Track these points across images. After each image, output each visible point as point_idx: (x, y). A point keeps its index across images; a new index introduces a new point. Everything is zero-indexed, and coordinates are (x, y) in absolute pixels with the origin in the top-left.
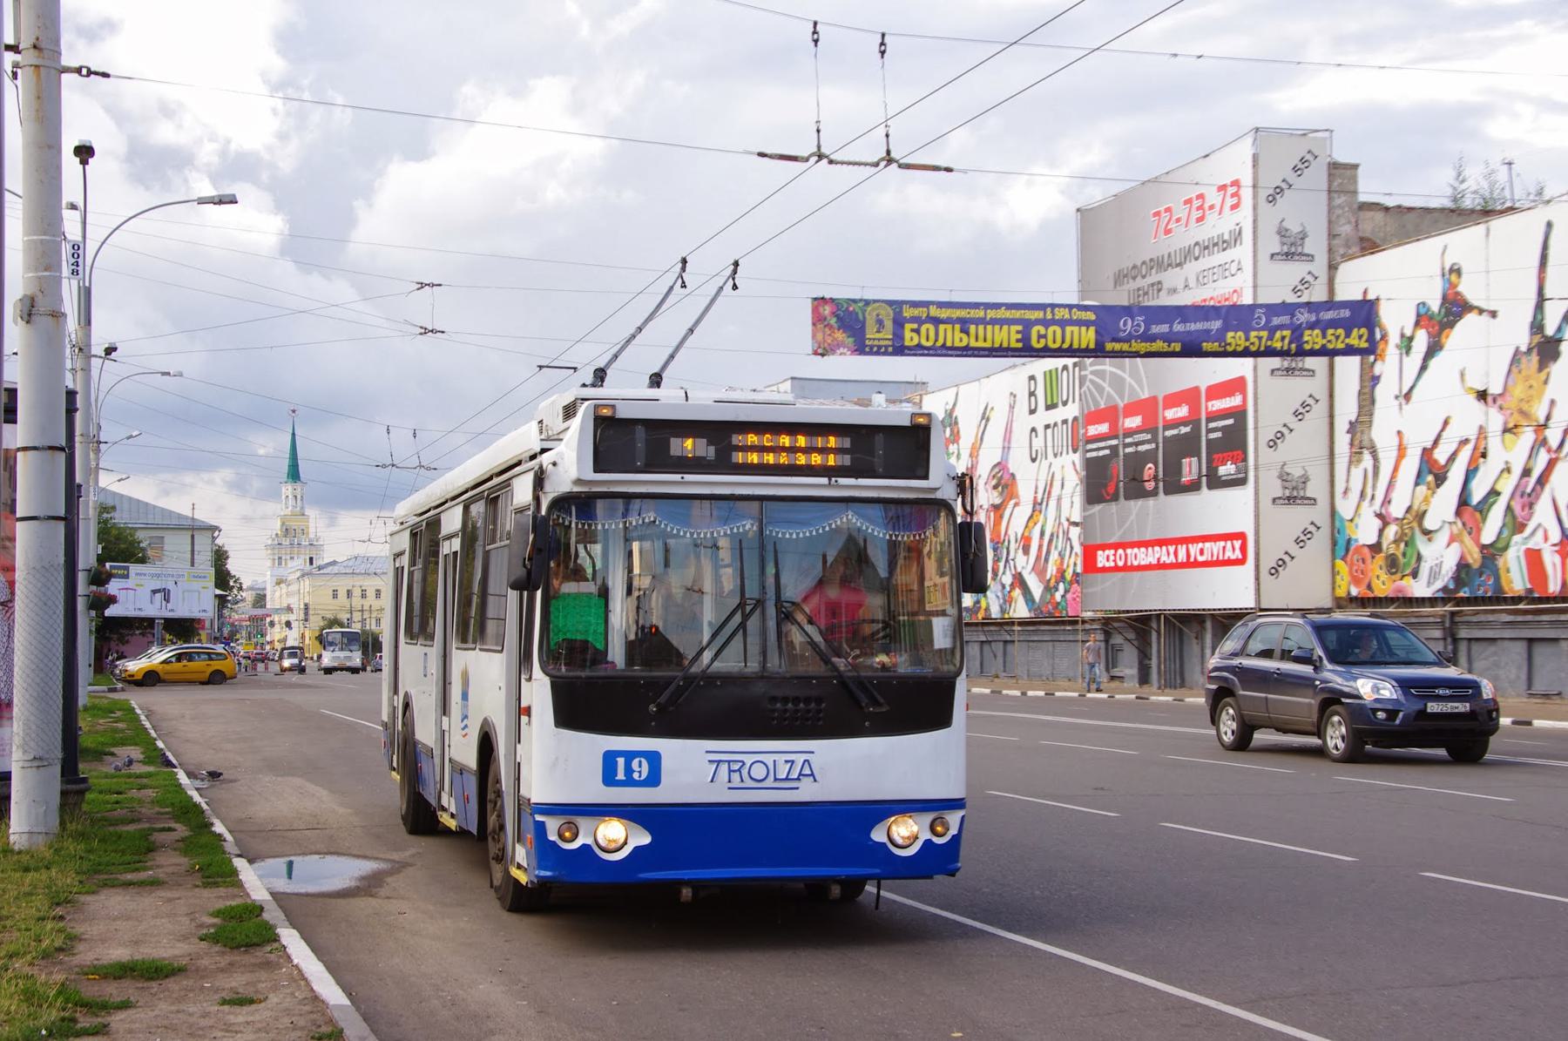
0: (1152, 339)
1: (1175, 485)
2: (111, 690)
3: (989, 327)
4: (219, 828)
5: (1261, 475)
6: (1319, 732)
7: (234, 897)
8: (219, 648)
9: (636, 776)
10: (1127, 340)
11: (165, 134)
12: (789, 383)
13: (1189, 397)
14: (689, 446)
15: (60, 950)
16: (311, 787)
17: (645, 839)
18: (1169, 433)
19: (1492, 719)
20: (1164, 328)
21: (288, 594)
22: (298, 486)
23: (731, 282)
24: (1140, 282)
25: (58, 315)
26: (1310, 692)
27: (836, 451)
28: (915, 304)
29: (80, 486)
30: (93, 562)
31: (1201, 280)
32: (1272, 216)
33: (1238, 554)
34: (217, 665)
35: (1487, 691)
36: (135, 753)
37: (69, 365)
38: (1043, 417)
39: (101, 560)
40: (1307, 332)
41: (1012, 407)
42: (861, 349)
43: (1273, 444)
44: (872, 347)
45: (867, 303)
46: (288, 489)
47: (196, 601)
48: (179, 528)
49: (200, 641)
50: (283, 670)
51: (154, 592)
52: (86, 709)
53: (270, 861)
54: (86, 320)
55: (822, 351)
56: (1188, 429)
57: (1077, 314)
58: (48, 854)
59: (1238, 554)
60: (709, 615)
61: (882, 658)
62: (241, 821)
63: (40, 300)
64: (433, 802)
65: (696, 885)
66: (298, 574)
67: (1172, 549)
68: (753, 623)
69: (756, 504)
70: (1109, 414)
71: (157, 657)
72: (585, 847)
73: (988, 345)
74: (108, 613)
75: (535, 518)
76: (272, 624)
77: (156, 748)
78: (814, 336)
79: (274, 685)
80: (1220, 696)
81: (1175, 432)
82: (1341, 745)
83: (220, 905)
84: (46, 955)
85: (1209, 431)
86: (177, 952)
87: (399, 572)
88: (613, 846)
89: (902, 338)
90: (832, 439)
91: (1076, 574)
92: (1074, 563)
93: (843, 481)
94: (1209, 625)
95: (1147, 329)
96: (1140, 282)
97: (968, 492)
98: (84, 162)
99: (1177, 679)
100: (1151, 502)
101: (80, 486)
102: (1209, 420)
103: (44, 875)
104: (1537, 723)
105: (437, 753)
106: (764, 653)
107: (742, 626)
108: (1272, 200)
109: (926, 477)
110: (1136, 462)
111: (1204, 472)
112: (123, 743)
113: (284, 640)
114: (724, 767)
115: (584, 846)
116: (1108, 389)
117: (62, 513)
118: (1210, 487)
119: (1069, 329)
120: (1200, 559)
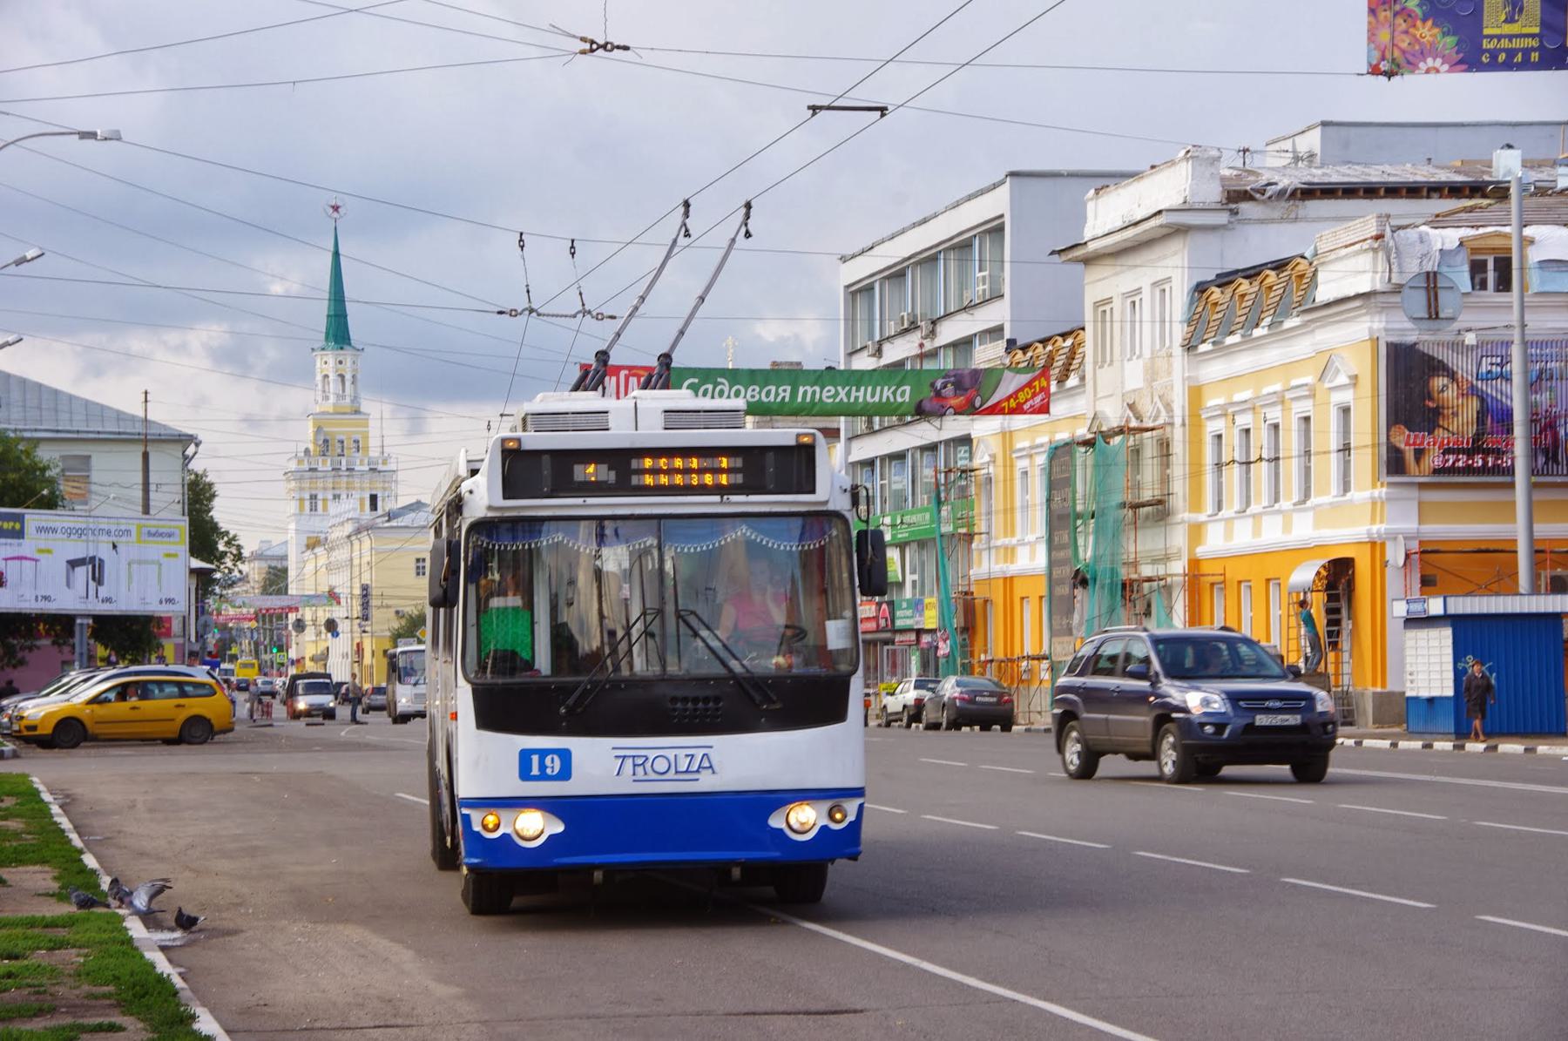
8: (200, 673)
9: (549, 771)
12: (1317, 132)
16: (380, 944)
17: (559, 828)
21: (329, 567)
22: (347, 356)
23: (743, 230)
27: (728, 471)
34: (196, 706)
36: (39, 877)
42: (1472, 58)
44: (1494, 54)
46: (326, 363)
47: (152, 581)
49: (162, 659)
50: (296, 715)
51: (73, 564)
62: (246, 1011)
66: (349, 528)
71: (81, 691)
72: (505, 836)
76: (300, 626)
77: (84, 870)
79: (305, 746)
97: (862, 500)
109: (813, 491)
112: (19, 858)
113: (323, 657)
114: (629, 762)
115: (504, 835)
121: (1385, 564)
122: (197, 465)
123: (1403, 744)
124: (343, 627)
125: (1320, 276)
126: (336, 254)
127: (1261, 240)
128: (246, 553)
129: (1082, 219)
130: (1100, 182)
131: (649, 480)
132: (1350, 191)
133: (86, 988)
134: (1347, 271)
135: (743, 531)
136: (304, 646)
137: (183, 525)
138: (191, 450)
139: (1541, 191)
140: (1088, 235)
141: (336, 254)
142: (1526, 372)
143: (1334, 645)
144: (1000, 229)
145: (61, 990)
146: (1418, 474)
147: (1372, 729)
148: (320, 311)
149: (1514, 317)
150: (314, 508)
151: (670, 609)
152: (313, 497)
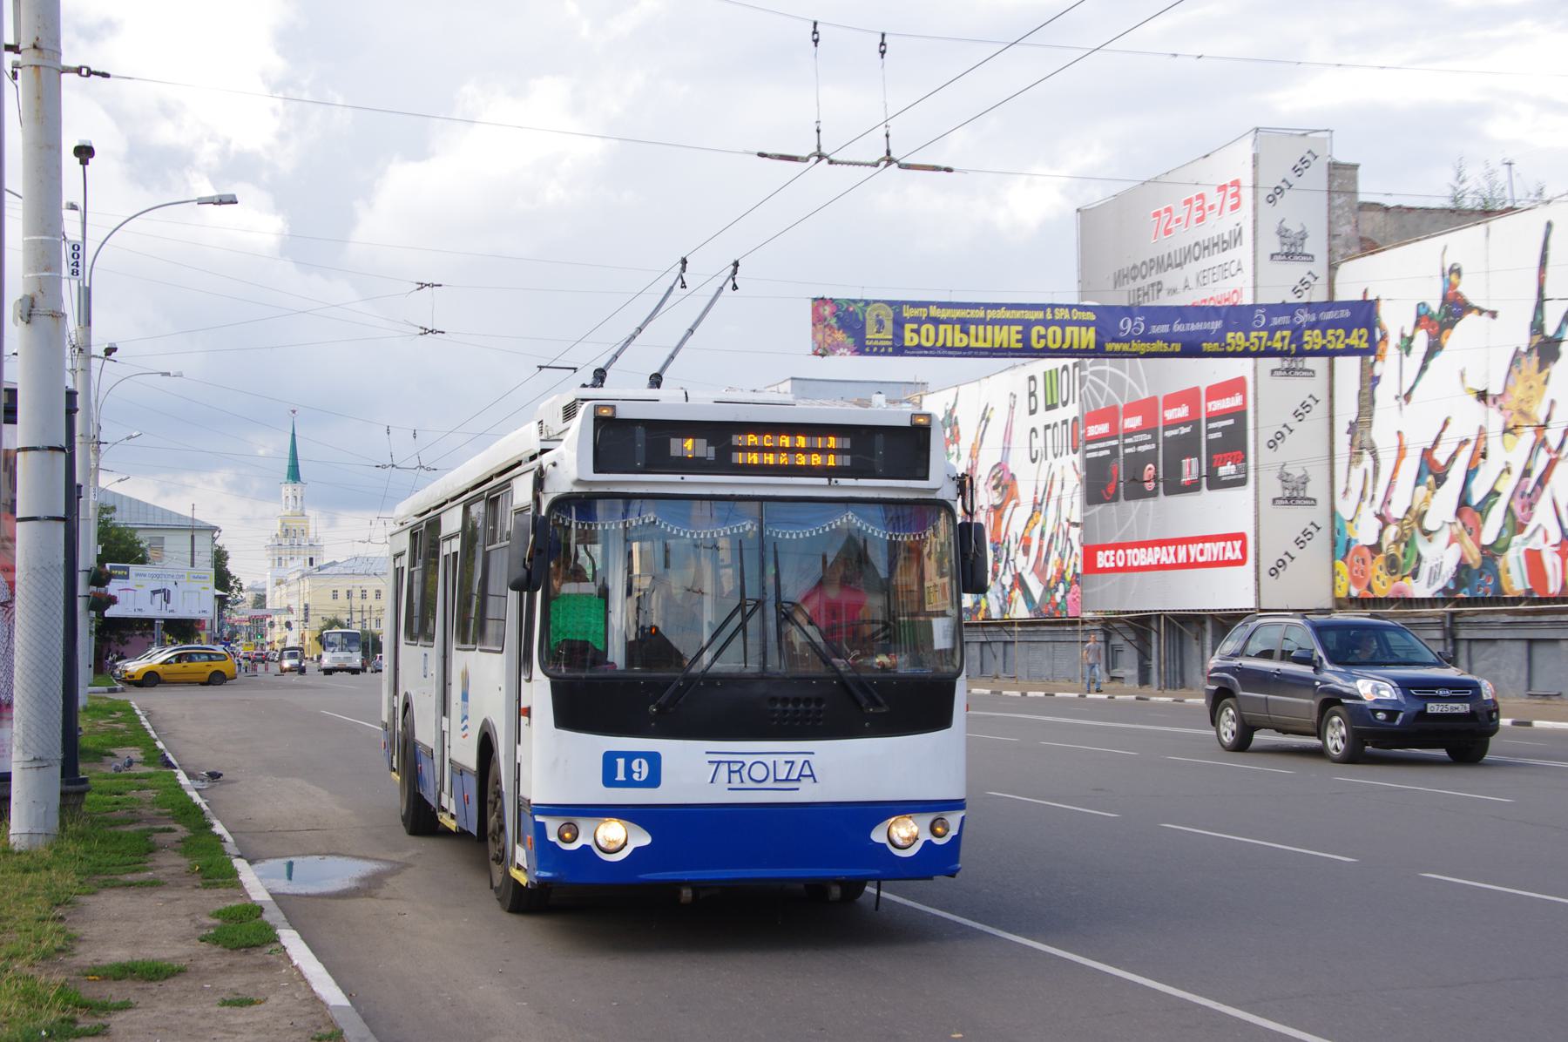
0: (1152, 339)
1: (1175, 486)
2: (111, 691)
3: (989, 328)
4: (219, 828)
5: (1261, 475)
6: (1319, 733)
7: (234, 897)
8: (219, 649)
9: (636, 777)
10: (1127, 340)
11: (165, 134)
13: (1189, 397)
14: (689, 446)
15: (60, 951)
17: (645, 840)
18: (1169, 434)
19: (1492, 720)
20: (1164, 328)
23: (731, 283)
24: (1140, 283)
25: (58, 316)
26: (1310, 692)
27: (836, 451)
28: (914, 305)
29: (80, 487)
30: (93, 562)
31: (1201, 280)
32: (1271, 217)
33: (1238, 555)
34: (217, 666)
35: (1487, 691)
36: (136, 753)
37: (68, 365)
38: (1043, 417)
39: (101, 560)
40: (1308, 332)
41: (1012, 408)
42: (861, 349)
43: (1273, 445)
44: (871, 347)
45: (867, 303)
46: (288, 490)
47: (195, 601)
48: (179, 529)
49: (200, 641)
50: (283, 671)
51: (154, 592)
52: (86, 709)
53: (271, 862)
54: (86, 320)
55: (822, 351)
56: (1188, 430)
57: (1077, 315)
58: (48, 855)
59: (1238, 555)
60: (709, 616)
61: (882, 659)
63: (39, 300)
64: (433, 803)
65: (696, 886)
66: (298, 575)
67: (1172, 549)
68: (753, 624)
69: (756, 505)
70: (1109, 415)
72: (585, 848)
73: (988, 345)
74: (108, 613)
75: (535, 518)
76: (272, 625)
77: (157, 749)
78: (814, 337)
80: (1220, 696)
81: (1175, 432)
82: (1341, 746)
83: (220, 906)
84: (46, 957)
85: (1209, 431)
86: (176, 953)
87: (399, 572)
88: (612, 847)
89: (902, 339)
90: (832, 439)
91: (1075, 575)
92: (1074, 563)
93: (842, 481)
94: (1209, 626)
95: (1147, 329)
96: (1140, 283)
98: (84, 162)
99: (1177, 680)
100: (1151, 502)
101: (80, 487)
102: (1209, 420)
103: (44, 876)
104: (1537, 724)
105: (437, 753)
106: (764, 654)
107: (742, 626)
108: (1272, 200)
109: (926, 478)
110: (1136, 463)
111: (1204, 472)
113: (284, 640)
114: (724, 768)
116: (1108, 389)
117: (62, 513)
118: (1210, 487)
119: (1068, 329)
120: (1200, 559)
122: (219, 542)
137: (212, 572)
148: (286, 463)
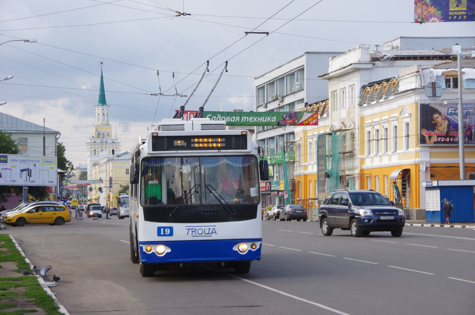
8: (61, 204)
9: (166, 233)
12: (399, 40)
17: (169, 250)
22: (105, 107)
23: (225, 69)
27: (220, 143)
36: (12, 266)
42: (446, 18)
44: (453, 16)
46: (99, 110)
47: (46, 176)
48: (36, 133)
49: (49, 200)
50: (90, 216)
51: (22, 171)
55: (420, 20)
65: (184, 263)
66: (106, 160)
69: (198, 158)
71: (25, 209)
72: (153, 253)
76: (91, 189)
78: (416, 11)
90: (219, 139)
93: (222, 151)
109: (246, 149)
113: (98, 199)
114: (191, 231)
121: (420, 171)
122: (59, 141)
123: (425, 225)
124: (104, 190)
125: (400, 84)
126: (102, 77)
127: (382, 73)
128: (74, 167)
129: (328, 66)
130: (333, 55)
131: (196, 145)
132: (409, 58)
133: (26, 299)
134: (408, 82)
135: (225, 161)
136: (92, 196)
138: (58, 136)
139: (467, 58)
140: (329, 71)
141: (102, 77)
142: (462, 112)
143: (404, 195)
144: (303, 69)
145: (19, 300)
146: (430, 143)
147: (415, 220)
148: (97, 94)
149: (459, 96)
150: (95, 154)
151: (203, 184)
152: (95, 150)
